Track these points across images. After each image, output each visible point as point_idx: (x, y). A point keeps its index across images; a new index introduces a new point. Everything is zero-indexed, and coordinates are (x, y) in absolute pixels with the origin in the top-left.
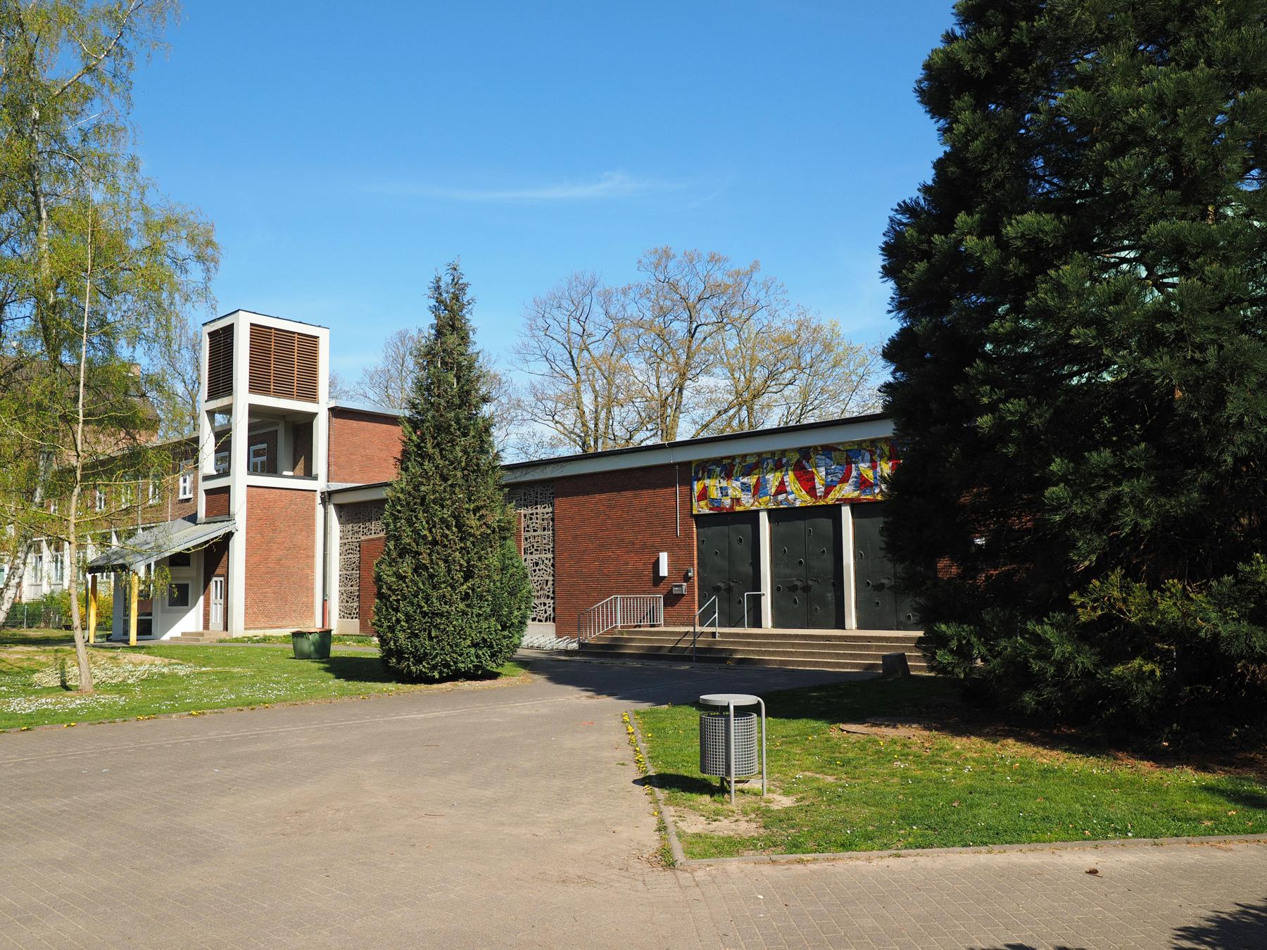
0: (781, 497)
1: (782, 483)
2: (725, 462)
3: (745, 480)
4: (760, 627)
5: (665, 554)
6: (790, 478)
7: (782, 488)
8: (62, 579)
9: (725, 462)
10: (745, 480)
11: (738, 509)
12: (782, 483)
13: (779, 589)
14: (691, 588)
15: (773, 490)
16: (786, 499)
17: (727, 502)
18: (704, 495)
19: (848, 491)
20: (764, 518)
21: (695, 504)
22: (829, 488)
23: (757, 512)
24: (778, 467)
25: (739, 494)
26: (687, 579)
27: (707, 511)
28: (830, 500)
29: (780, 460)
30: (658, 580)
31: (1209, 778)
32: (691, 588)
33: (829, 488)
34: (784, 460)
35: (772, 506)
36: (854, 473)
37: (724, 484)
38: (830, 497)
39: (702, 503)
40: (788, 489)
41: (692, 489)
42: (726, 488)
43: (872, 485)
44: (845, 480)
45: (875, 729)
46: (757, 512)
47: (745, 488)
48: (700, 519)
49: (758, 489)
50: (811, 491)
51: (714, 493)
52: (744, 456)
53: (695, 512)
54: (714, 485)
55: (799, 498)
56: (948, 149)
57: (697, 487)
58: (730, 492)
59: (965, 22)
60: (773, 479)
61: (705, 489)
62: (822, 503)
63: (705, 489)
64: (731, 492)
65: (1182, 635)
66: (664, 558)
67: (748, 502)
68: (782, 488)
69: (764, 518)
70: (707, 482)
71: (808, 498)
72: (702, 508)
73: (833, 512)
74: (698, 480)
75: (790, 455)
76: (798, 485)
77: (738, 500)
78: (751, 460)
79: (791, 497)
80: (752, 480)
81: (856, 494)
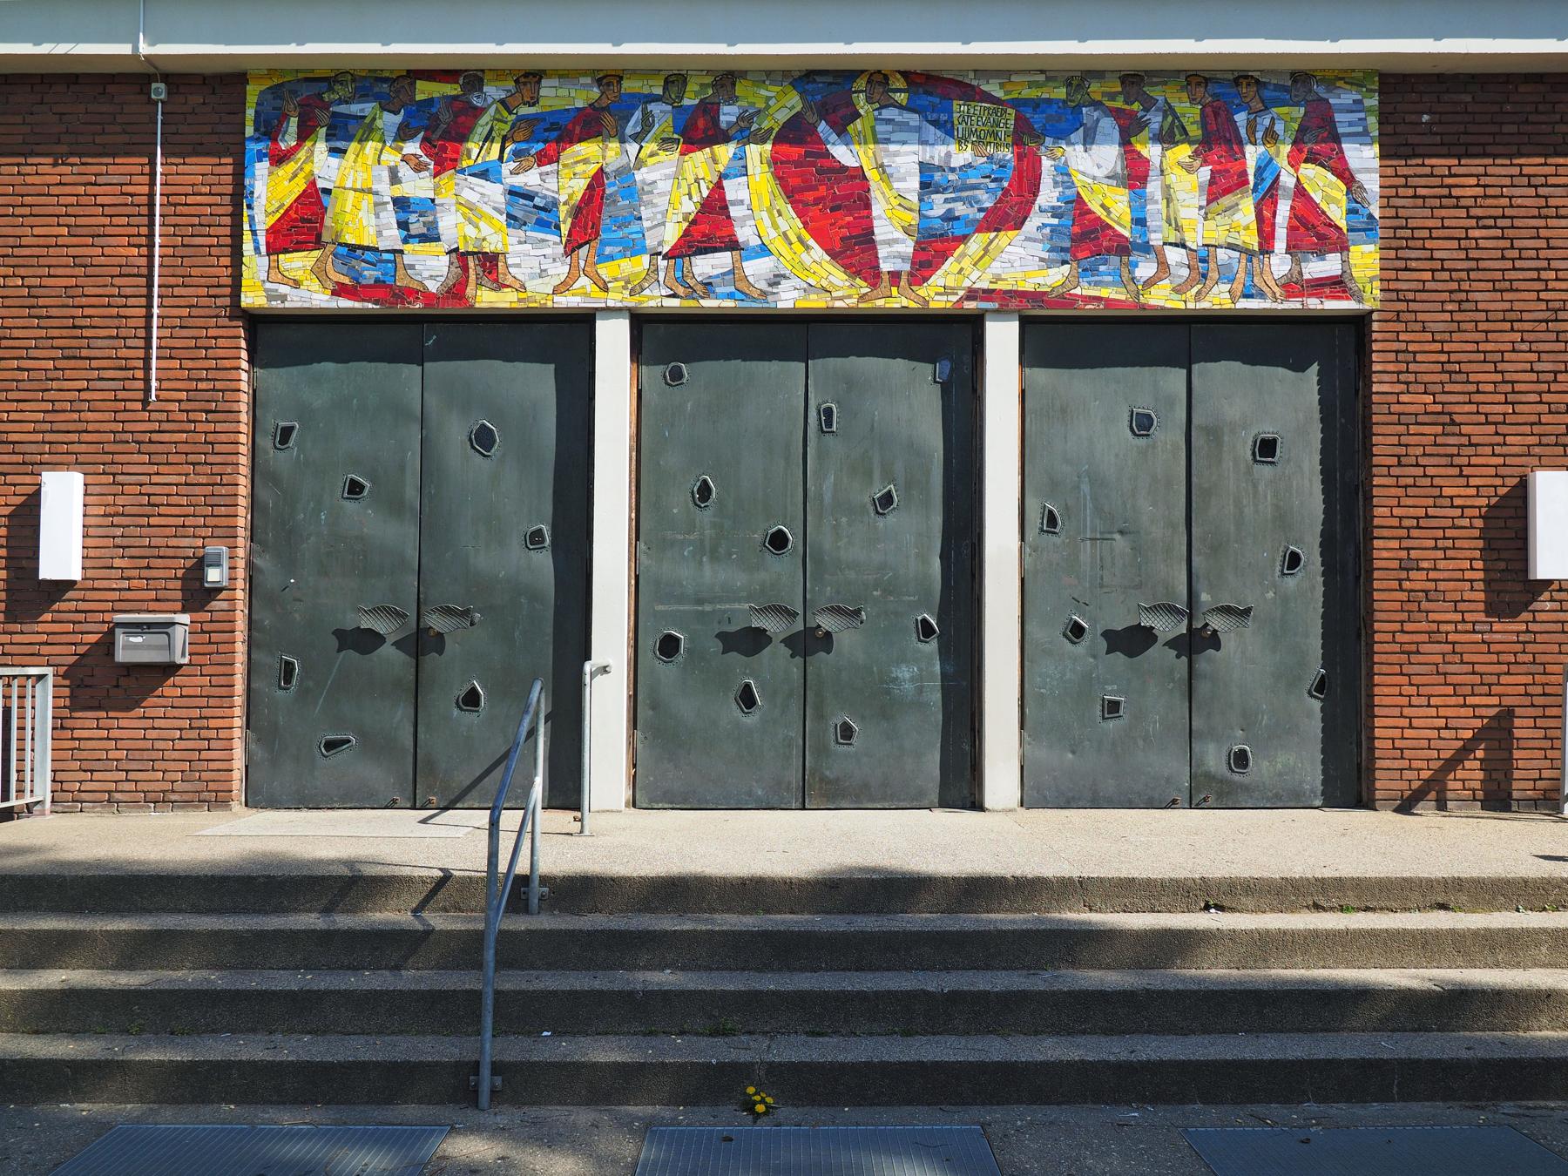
0: (706, 266)
1: (715, 207)
2: (425, 90)
3: (531, 179)
5: (76, 480)
6: (756, 196)
7: (711, 227)
9: (425, 90)
10: (531, 179)
11: (486, 299)
12: (715, 207)
13: (669, 646)
14: (210, 640)
15: (671, 234)
16: (733, 273)
18: (304, 224)
19: (1020, 261)
20: (612, 340)
21: (255, 265)
22: (933, 248)
23: (584, 322)
24: (698, 132)
25: (494, 235)
26: (197, 595)
28: (940, 291)
29: (709, 109)
30: (34, 596)
31: (43, 857)
32: (210, 640)
33: (933, 248)
34: (728, 115)
35: (656, 299)
36: (1048, 195)
37: (417, 186)
38: (938, 279)
39: (297, 263)
40: (744, 234)
41: (239, 195)
43: (1123, 248)
44: (1006, 216)
46: (584, 322)
47: (527, 211)
48: (276, 336)
49: (590, 222)
50: (855, 250)
51: (362, 222)
52: (530, 76)
53: (252, 298)
54: (364, 181)
55: (804, 277)
57: (271, 191)
60: (669, 183)
61: (313, 201)
62: (897, 301)
63: (313, 201)
64: (475, 224)
65: (1107, 300)
66: (64, 499)
67: (537, 275)
68: (711, 227)
69: (612, 340)
70: (320, 162)
71: (838, 277)
72: (303, 284)
73: (951, 340)
74: (279, 159)
75: (750, 95)
76: (791, 222)
77: (490, 262)
78: (554, 97)
79: (756, 269)
80: (564, 181)
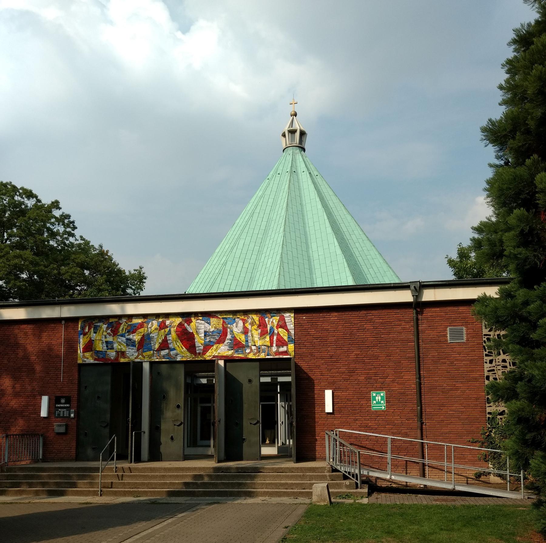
0: (164, 353)
2: (111, 320)
4: (188, 447)
8: (418, 463)
11: (122, 360)
15: (157, 346)
16: (169, 354)
17: (112, 354)
18: (89, 347)
27: (92, 361)
28: (208, 356)
38: (208, 354)
39: (87, 354)
40: (171, 346)
42: (112, 343)
44: (221, 341)
45: (213, 498)
47: (130, 343)
51: (100, 347)
56: (494, 219)
58: (116, 346)
59: (523, 463)
62: (200, 358)
71: (188, 354)
81: (230, 353)
